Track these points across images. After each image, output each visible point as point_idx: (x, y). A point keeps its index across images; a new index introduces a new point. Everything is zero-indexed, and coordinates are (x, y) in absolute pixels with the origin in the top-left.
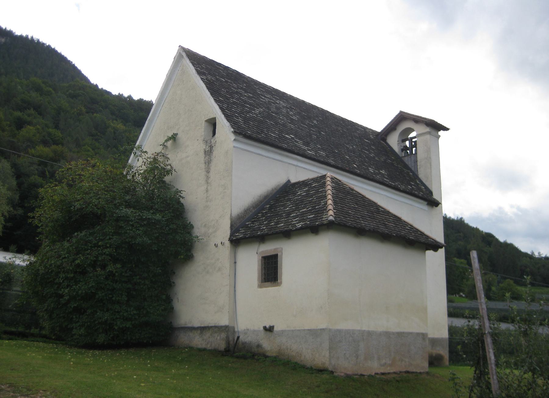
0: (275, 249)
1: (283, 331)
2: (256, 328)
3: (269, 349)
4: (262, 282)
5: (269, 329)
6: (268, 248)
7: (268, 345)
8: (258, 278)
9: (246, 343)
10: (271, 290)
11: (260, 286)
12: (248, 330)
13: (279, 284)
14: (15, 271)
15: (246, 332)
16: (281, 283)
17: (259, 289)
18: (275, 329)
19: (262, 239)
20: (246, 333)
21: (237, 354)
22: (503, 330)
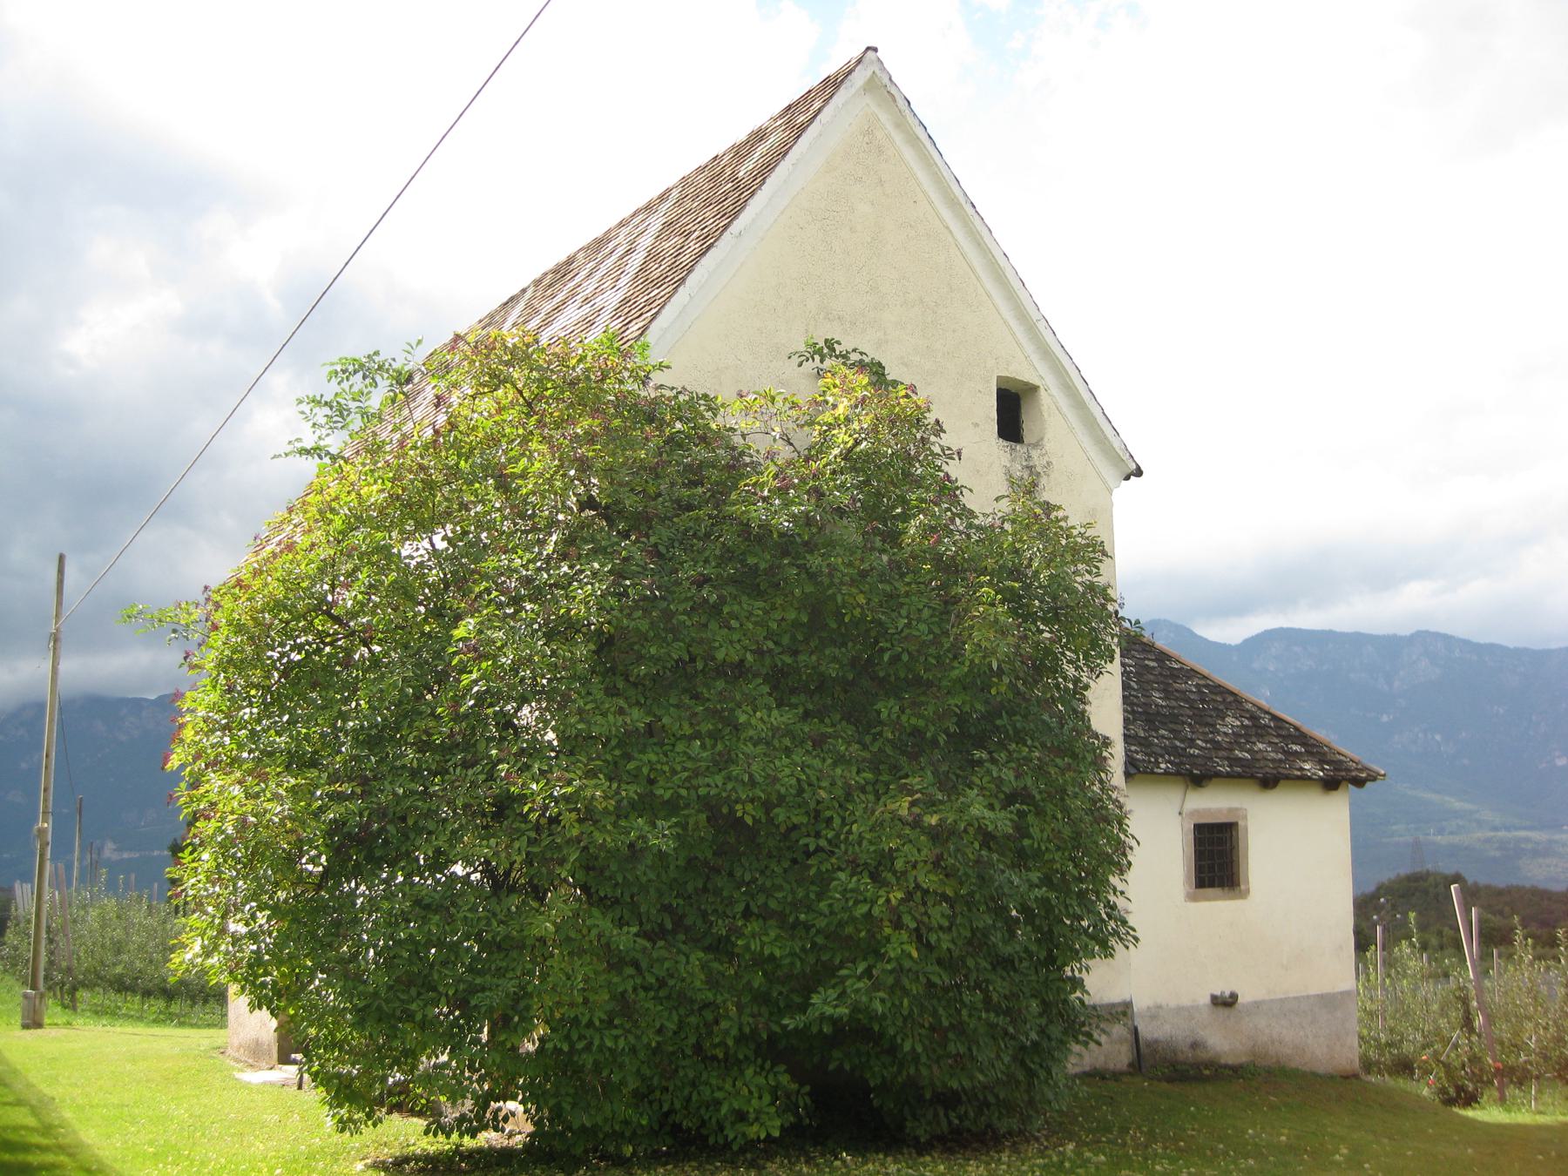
0: (1230, 810)
1: (1257, 1005)
2: (1185, 1001)
3: (1226, 1048)
4: (1192, 890)
5: (1225, 1003)
6: (1214, 802)
7: (1222, 1042)
8: (1188, 877)
9: (1156, 1041)
10: (1218, 909)
11: (1192, 898)
12: (1160, 1007)
13: (1244, 895)
14: (1080, 1055)
15: (1155, 1013)
16: (1248, 891)
17: (1193, 905)
18: (1240, 1000)
19: (1198, 779)
20: (1154, 1017)
21: (1176, 1076)
22: (990, 534)
